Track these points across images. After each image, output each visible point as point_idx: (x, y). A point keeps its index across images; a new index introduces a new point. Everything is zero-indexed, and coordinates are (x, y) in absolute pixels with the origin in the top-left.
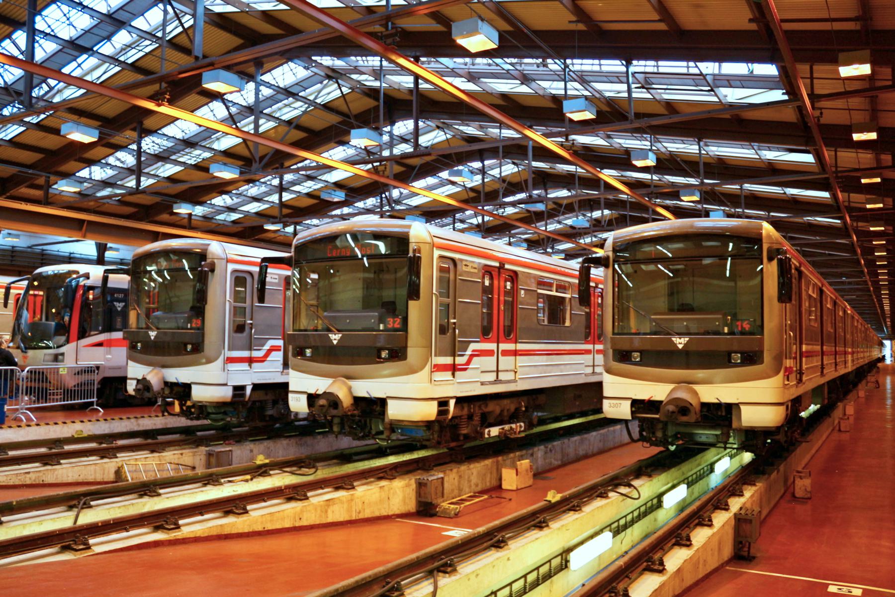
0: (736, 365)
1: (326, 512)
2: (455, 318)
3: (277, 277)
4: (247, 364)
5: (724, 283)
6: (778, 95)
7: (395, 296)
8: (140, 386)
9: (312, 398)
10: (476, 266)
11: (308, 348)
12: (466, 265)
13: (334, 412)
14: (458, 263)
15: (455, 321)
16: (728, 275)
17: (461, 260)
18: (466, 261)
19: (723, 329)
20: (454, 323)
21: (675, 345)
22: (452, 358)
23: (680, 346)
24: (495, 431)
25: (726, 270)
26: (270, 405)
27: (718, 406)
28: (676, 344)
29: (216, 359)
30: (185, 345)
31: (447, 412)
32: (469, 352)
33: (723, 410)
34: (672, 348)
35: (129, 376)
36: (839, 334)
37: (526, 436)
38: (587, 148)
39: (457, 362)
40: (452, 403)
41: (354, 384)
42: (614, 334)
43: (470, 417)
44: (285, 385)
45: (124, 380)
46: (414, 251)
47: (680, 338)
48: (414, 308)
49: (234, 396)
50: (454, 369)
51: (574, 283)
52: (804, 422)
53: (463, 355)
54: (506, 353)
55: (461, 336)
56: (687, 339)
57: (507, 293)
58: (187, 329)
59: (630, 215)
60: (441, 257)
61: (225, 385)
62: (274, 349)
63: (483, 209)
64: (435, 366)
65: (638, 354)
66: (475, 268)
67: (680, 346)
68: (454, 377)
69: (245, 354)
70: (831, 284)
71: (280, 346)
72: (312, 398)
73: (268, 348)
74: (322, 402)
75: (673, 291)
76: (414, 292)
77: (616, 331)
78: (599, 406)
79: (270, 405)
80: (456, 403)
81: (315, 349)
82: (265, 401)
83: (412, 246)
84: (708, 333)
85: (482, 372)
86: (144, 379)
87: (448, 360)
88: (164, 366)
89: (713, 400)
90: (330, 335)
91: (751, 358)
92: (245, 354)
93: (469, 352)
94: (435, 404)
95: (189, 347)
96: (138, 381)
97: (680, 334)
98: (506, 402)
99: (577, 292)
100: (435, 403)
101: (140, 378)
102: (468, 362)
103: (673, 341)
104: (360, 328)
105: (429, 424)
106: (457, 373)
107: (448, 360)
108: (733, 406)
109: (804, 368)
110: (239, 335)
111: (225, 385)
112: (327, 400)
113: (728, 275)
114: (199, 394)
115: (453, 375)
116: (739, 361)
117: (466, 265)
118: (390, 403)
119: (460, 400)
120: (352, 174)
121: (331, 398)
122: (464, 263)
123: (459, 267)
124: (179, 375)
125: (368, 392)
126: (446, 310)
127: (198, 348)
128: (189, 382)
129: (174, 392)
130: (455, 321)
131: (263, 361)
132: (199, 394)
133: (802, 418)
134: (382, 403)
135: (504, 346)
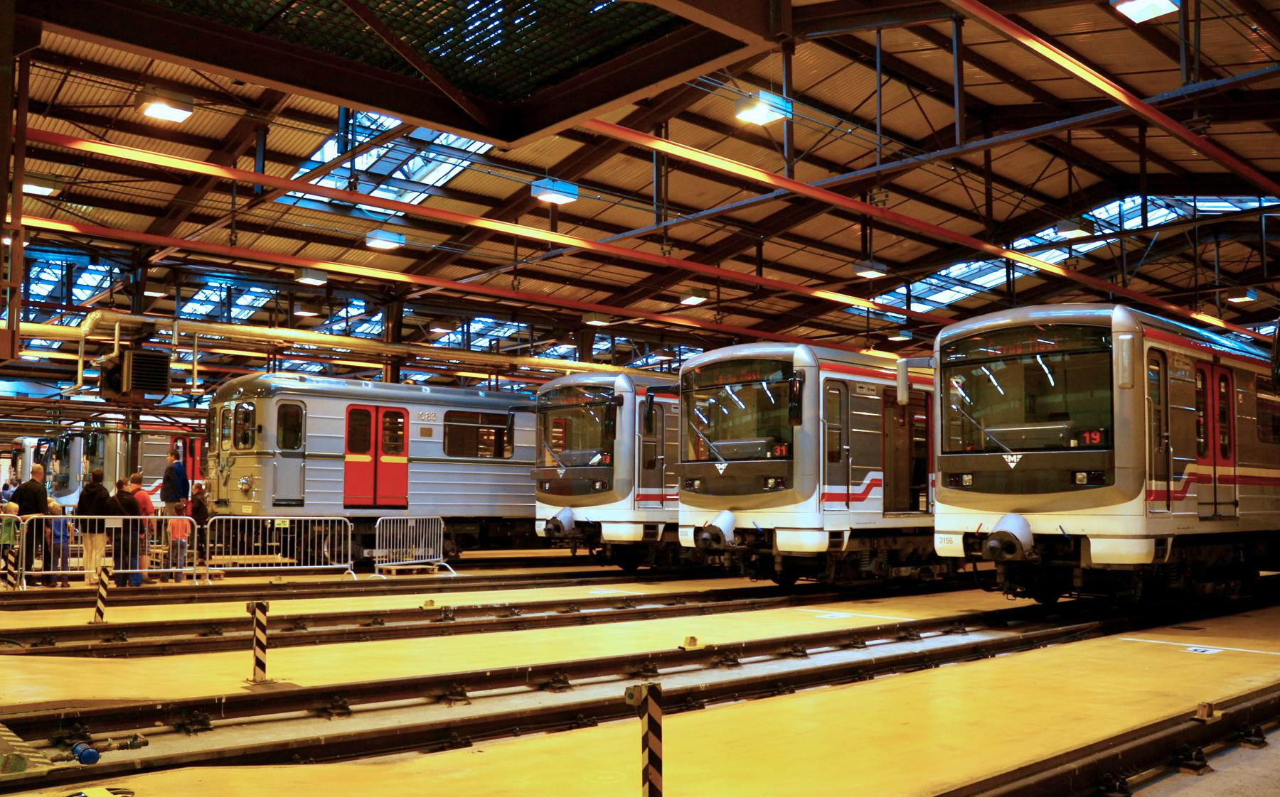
0: (1081, 487)
2: (1167, 431)
3: (874, 387)
4: (659, 502)
6: (143, 418)
7: (1066, 402)
8: (550, 526)
9: (698, 531)
11: (771, 478)
13: (557, 534)
15: (848, 447)
17: (1174, 353)
20: (848, 450)
22: (846, 487)
26: (866, 559)
27: (587, 524)
28: (1007, 463)
30: (766, 480)
31: (841, 544)
32: (867, 481)
35: (538, 517)
38: (724, 307)
42: (943, 453)
44: (932, 528)
45: (532, 521)
47: (1012, 455)
49: (646, 535)
52: (117, 499)
54: (1225, 480)
56: (1020, 457)
57: (1222, 396)
60: (828, 380)
61: (821, 529)
62: (874, 483)
63: (647, 364)
64: (824, 495)
65: (1085, 474)
68: (848, 508)
69: (840, 489)
71: (880, 480)
72: (698, 531)
73: (869, 482)
74: (706, 535)
76: (796, 416)
79: (866, 559)
82: (861, 552)
83: (795, 369)
85: (1199, 504)
86: (554, 518)
88: (573, 506)
90: (1005, 457)
91: (1101, 478)
92: (840, 489)
93: (867, 481)
95: (598, 485)
96: (548, 522)
100: (641, 526)
101: (549, 518)
102: (1185, 490)
104: (1042, 446)
105: (819, 556)
110: (651, 471)
111: (821, 529)
114: (609, 533)
115: (848, 505)
118: (778, 533)
119: (1180, 540)
122: (858, 385)
123: (1170, 361)
124: (586, 514)
127: (607, 486)
128: (772, 527)
129: (746, 542)
130: (848, 447)
131: (862, 500)
132: (609, 533)
133: (113, 497)
134: (770, 533)
135: (1223, 471)
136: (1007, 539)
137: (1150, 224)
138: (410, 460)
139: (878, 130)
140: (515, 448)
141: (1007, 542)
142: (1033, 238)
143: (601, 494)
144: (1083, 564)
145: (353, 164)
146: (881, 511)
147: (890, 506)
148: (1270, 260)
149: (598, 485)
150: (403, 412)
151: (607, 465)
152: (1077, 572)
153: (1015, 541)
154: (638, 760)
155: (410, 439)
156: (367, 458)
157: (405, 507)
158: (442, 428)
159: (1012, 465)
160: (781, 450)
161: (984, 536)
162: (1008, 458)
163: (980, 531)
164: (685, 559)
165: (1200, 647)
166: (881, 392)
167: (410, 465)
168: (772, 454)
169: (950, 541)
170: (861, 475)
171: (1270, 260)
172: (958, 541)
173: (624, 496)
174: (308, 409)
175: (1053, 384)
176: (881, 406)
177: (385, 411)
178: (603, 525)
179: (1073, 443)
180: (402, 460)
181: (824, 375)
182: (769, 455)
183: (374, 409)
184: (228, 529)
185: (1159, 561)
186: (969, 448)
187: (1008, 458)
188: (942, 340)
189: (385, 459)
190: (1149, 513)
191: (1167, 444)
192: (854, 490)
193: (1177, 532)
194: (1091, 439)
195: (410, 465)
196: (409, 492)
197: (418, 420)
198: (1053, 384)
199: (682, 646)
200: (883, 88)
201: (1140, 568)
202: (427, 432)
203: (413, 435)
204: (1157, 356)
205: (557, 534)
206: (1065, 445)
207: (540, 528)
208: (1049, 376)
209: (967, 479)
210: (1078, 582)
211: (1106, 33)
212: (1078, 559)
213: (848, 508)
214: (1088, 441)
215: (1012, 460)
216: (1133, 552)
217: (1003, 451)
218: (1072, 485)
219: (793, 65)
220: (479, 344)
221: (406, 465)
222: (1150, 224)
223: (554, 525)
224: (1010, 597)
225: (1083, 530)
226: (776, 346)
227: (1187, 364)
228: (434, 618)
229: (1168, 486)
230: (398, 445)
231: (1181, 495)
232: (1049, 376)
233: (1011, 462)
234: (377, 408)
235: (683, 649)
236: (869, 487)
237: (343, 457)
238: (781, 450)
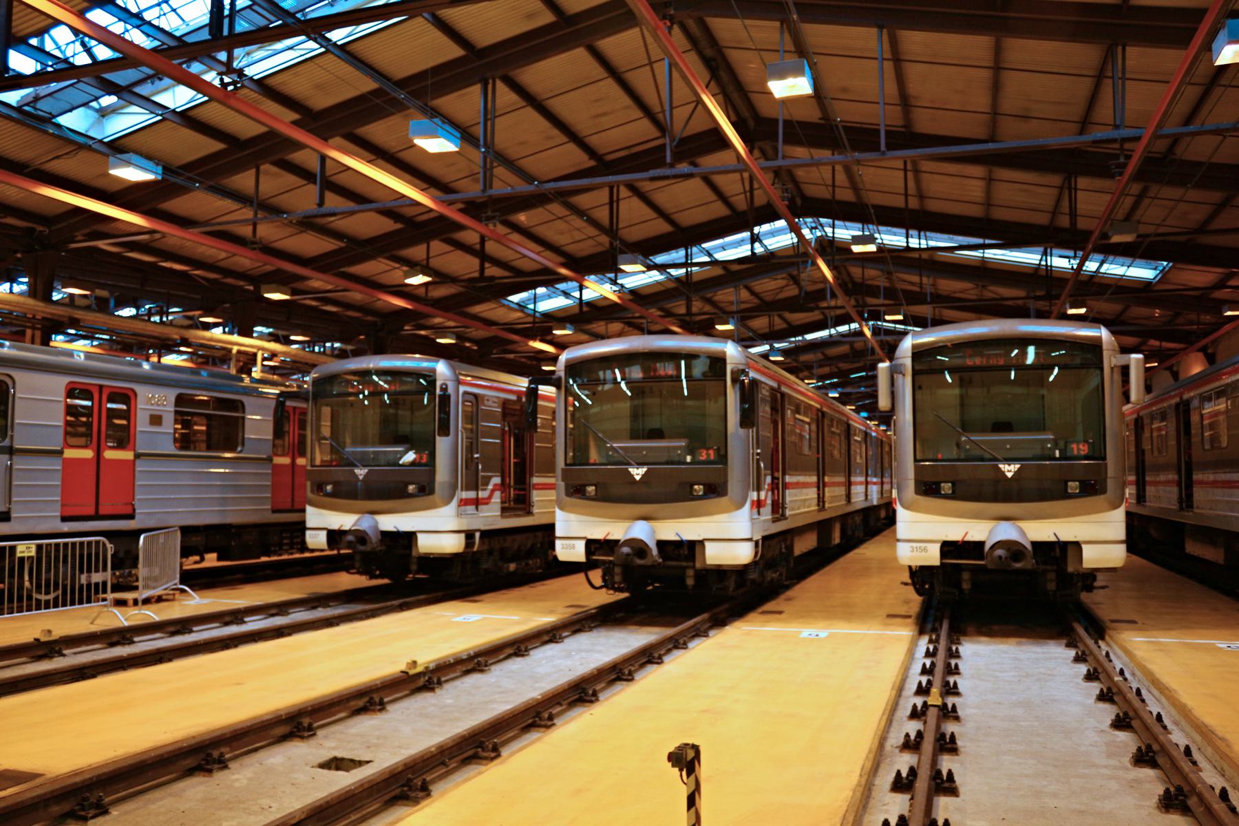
2: (477, 453)
5: (1007, 389)
10: (496, 400)
11: (412, 484)
12: (488, 400)
14: (479, 399)
16: (686, 394)
18: (488, 396)
19: (685, 458)
20: (477, 458)
21: (1003, 473)
23: (1009, 475)
24: (512, 567)
25: (683, 388)
27: (679, 544)
32: (490, 487)
33: (686, 548)
36: (832, 455)
37: (259, 558)
39: (480, 496)
40: (477, 535)
41: (658, 525)
43: (490, 552)
46: (442, 389)
47: (1009, 465)
48: (442, 445)
50: (477, 502)
51: (202, 431)
53: (485, 490)
55: (483, 470)
56: (1018, 466)
58: (1055, 459)
60: (465, 393)
64: (461, 500)
65: (950, 484)
66: (495, 403)
67: (1009, 475)
75: (636, 415)
77: (568, 462)
78: (469, 541)
80: (481, 537)
81: (336, 484)
84: (672, 463)
87: (471, 494)
89: (391, 529)
90: (630, 470)
91: (715, 490)
93: (490, 487)
97: (1009, 460)
98: (519, 537)
100: (463, 535)
103: (1000, 469)
106: (480, 507)
107: (471, 494)
108: (697, 543)
109: (787, 502)
113: (686, 394)
116: (701, 493)
117: (488, 400)
118: (707, 544)
119: (485, 534)
125: (677, 534)
126: (471, 448)
136: (1016, 548)
138: (138, 456)
139: (255, 205)
140: (246, 441)
141: (360, 537)
142: (551, 288)
143: (417, 499)
144: (698, 565)
145: (231, 58)
146: (499, 513)
147: (505, 510)
148: (234, 351)
149: (411, 488)
150: (131, 394)
151: (425, 465)
152: (690, 572)
153: (366, 537)
155: (139, 429)
156: (88, 454)
157: (131, 516)
158: (173, 414)
159: (638, 478)
160: (708, 455)
161: (343, 533)
162: (357, 471)
163: (966, 539)
164: (486, 570)
165: (814, 632)
166: (501, 403)
167: (138, 462)
168: (692, 459)
169: (925, 550)
170: (486, 481)
171: (234, 351)
172: (581, 546)
173: (448, 501)
174: (17, 385)
176: (500, 417)
177: (110, 390)
178: (420, 536)
179: (689, 459)
180: (127, 455)
181: (462, 389)
182: (689, 459)
183: (97, 388)
184: (48, 556)
185: (469, 550)
186: (334, 463)
188: (567, 361)
189: (109, 454)
190: (459, 515)
191: (758, 460)
192: (482, 494)
193: (483, 528)
194: (1079, 449)
195: (138, 462)
196: (137, 497)
197: (147, 404)
199: (37, 636)
201: (456, 555)
202: (156, 420)
203: (142, 424)
204: (471, 398)
205: (362, 548)
206: (682, 460)
207: (316, 540)
209: (946, 488)
210: (414, 567)
211: (646, 139)
212: (693, 560)
214: (1076, 452)
216: (452, 544)
217: (356, 466)
218: (1065, 496)
219: (497, 98)
220: (779, 281)
221: (132, 464)
223: (334, 536)
224: (612, 592)
225: (1076, 537)
226: (1063, 326)
227: (495, 403)
229: (478, 494)
230: (123, 439)
231: (486, 501)
233: (1008, 471)
234: (101, 387)
235: (407, 673)
236: (493, 491)
237: (61, 452)
238: (708, 455)
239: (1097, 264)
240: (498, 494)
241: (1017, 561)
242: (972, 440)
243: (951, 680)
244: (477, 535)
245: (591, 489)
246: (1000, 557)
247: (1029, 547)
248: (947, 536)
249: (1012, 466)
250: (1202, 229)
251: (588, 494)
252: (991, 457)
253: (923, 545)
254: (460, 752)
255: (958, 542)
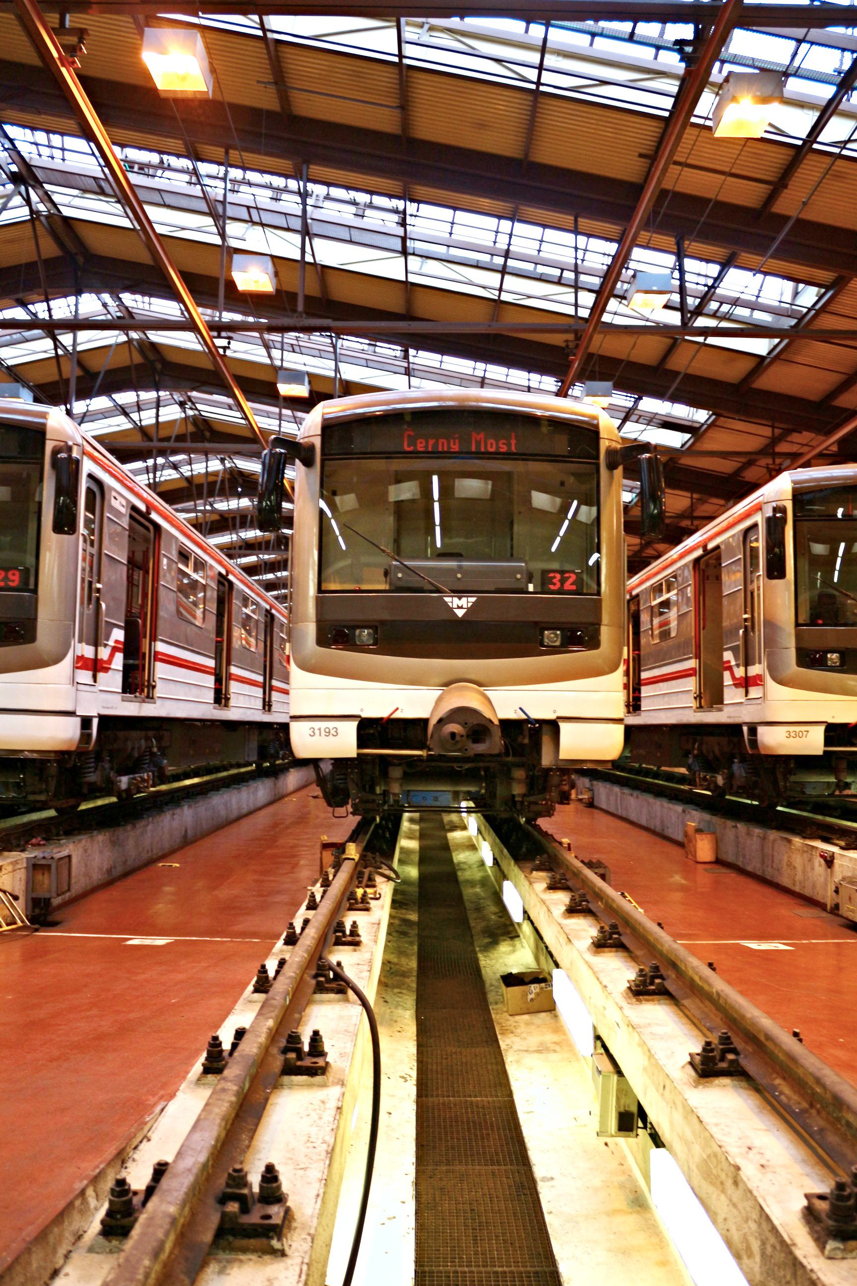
1: (675, 1087)
21: (451, 610)
23: (460, 613)
29: (57, 659)
34: (445, 616)
40: (95, 722)
47: (460, 598)
56: (473, 599)
59: (708, 216)
61: (71, 714)
67: (460, 613)
68: (95, 681)
70: (194, 617)
94: (75, 722)
97: (459, 592)
99: (123, 617)
111: (71, 714)
112: (464, 724)
118: (564, 727)
120: (250, 16)
121: (473, 721)
134: (553, 726)
137: (606, 318)
154: (80, 306)
162: (453, 602)
172: (349, 731)
175: (344, 548)
187: (453, 602)
198: (344, 548)
200: (245, 209)
208: (340, 539)
213: (95, 681)
215: (460, 605)
222: (606, 318)
228: (141, 635)
232: (340, 539)
233: (459, 607)
236: (115, 650)
239: (721, 309)
240: (119, 658)
241: (476, 741)
242: (405, 566)
243: (350, 918)
244: (95, 722)
245: (833, 657)
246: (453, 735)
247: (496, 722)
248: (362, 710)
249: (464, 600)
250: (115, 196)
251: (829, 663)
252: (433, 588)
253: (331, 724)
254: (696, 1021)
255: (382, 719)
